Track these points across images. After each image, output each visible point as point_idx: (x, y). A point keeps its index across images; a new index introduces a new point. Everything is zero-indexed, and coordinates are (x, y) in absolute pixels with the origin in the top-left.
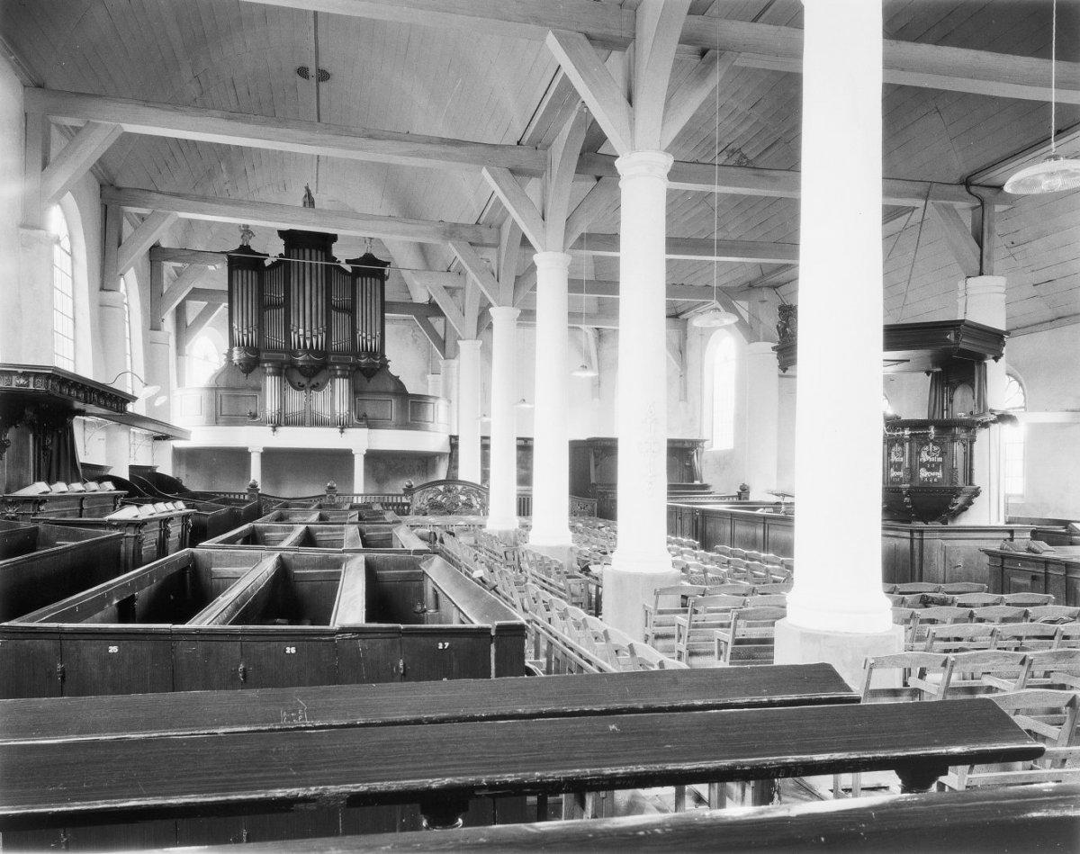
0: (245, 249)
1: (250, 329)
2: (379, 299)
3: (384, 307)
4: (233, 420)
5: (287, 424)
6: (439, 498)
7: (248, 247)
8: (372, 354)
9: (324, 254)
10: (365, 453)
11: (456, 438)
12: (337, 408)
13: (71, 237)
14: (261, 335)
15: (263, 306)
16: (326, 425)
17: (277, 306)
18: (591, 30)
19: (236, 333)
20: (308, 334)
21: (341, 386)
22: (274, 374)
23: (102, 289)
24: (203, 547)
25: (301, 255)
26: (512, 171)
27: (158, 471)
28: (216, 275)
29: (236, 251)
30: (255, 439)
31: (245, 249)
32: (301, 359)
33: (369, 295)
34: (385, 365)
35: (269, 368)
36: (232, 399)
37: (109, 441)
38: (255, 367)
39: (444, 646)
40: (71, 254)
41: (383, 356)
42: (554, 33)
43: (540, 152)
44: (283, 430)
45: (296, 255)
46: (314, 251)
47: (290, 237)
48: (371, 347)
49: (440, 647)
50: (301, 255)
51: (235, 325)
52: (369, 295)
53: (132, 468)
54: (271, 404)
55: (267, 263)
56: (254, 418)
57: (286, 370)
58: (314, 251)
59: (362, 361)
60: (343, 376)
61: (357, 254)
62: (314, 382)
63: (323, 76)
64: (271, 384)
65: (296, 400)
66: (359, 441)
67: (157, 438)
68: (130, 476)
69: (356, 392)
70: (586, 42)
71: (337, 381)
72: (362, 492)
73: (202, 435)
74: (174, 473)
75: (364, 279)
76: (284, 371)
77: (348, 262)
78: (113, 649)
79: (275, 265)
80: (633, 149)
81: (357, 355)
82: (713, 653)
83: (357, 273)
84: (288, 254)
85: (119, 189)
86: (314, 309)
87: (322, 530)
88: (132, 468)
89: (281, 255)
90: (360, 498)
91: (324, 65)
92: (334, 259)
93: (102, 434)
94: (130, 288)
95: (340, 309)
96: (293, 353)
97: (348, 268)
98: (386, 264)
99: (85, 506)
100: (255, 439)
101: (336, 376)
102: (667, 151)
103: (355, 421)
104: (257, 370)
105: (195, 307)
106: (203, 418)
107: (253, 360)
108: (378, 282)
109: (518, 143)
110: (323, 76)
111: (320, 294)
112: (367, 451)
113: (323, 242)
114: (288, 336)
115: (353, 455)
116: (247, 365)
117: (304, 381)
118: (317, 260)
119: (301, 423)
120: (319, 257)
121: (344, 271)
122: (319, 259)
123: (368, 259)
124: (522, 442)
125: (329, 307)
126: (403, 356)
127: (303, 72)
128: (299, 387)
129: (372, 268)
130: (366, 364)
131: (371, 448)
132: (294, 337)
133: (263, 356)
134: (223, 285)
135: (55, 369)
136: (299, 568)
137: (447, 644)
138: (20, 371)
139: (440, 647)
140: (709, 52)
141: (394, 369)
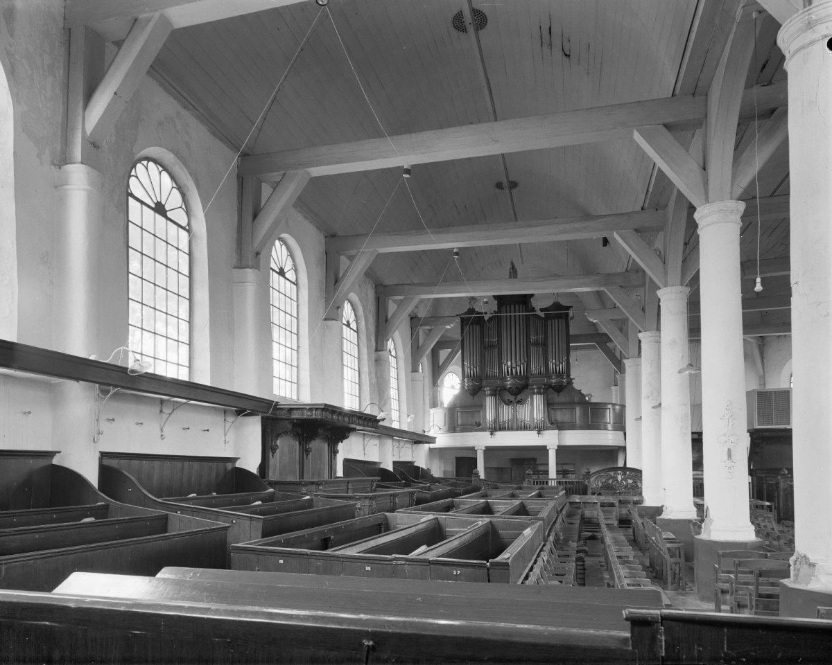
0: (471, 311)
1: (522, 360)
2: (564, 334)
3: (569, 338)
4: (466, 428)
5: (501, 429)
6: (610, 481)
7: (473, 309)
8: (560, 375)
9: (524, 306)
10: (484, 449)
11: (700, 434)
12: (535, 417)
13: (357, 320)
14: (482, 369)
15: (485, 347)
16: (527, 430)
17: (493, 346)
18: (667, 121)
19: (466, 369)
20: (514, 365)
21: (538, 400)
22: (491, 395)
23: (377, 350)
24: (399, 512)
25: (513, 309)
26: (637, 230)
27: (415, 464)
28: (452, 328)
29: (466, 313)
30: (480, 441)
31: (471, 311)
32: (509, 383)
33: (557, 332)
34: (570, 382)
35: (487, 391)
36: (464, 415)
37: (381, 446)
38: (479, 391)
39: (457, 573)
40: (357, 332)
41: (568, 376)
42: (637, 130)
43: (660, 211)
44: (499, 434)
45: (505, 311)
46: (517, 306)
47: (502, 300)
48: (516, 372)
49: (455, 573)
50: (513, 309)
51: (465, 363)
52: (557, 332)
53: (395, 463)
54: (489, 415)
55: (486, 318)
56: (478, 427)
57: (499, 391)
58: (517, 306)
59: (553, 381)
60: (539, 393)
61: (548, 303)
62: (519, 398)
63: (513, 185)
64: (489, 402)
65: (507, 413)
66: (551, 440)
67: (415, 443)
68: (394, 468)
69: (549, 405)
70: (664, 129)
71: (535, 396)
72: (555, 477)
73: (443, 440)
74: (426, 464)
75: (553, 321)
76: (498, 392)
77: (542, 310)
78: (281, 561)
79: (490, 319)
80: (707, 200)
81: (550, 377)
82: (747, 606)
83: (548, 317)
84: (500, 311)
85: (386, 286)
86: (526, 344)
87: (499, 504)
88: (395, 463)
89: (495, 312)
90: (553, 481)
91: (512, 179)
92: (533, 310)
93: (376, 442)
94: (397, 345)
95: (536, 344)
96: (504, 379)
97: (542, 314)
98: (568, 308)
99: (350, 487)
100: (480, 441)
101: (534, 393)
102: (740, 199)
103: (549, 425)
104: (480, 393)
105: (443, 354)
106: (445, 428)
107: (475, 389)
108: (564, 321)
109: (642, 209)
110: (513, 185)
111: (522, 337)
112: (558, 446)
113: (524, 300)
114: (500, 368)
115: (548, 450)
116: (474, 390)
117: (512, 398)
118: (510, 312)
119: (511, 429)
120: (517, 309)
121: (539, 317)
122: (521, 310)
123: (557, 306)
124: (696, 436)
125: (528, 343)
126: (586, 375)
127: (499, 186)
128: (509, 403)
129: (559, 312)
130: (555, 383)
131: (563, 444)
132: (505, 368)
133: (484, 383)
134: (458, 336)
135: (326, 405)
136: (504, 529)
137: (459, 572)
138: (308, 407)
139: (455, 573)
140: (778, 110)
141: (577, 385)
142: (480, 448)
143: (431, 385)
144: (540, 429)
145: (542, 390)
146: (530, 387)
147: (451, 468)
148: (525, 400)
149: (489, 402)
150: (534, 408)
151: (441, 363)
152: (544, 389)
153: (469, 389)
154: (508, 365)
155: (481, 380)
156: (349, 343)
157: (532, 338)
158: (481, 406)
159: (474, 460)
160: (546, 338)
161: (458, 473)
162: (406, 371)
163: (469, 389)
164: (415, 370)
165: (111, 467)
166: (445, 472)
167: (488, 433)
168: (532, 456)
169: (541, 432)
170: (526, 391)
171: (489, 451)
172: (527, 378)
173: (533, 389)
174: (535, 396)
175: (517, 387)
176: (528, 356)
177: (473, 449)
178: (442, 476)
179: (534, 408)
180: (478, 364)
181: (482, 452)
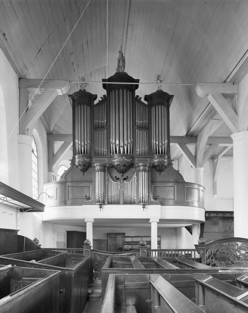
1: (126, 142)
4: (75, 202)
8: (162, 154)
9: (104, 173)
15: (95, 128)
27: (19, 233)
30: (89, 213)
51: (76, 141)
56: (87, 200)
57: (108, 168)
64: (98, 177)
65: (115, 188)
69: (152, 182)
90: (154, 252)
95: (142, 128)
100: (89, 213)
103: (152, 200)
104: (90, 169)
106: (58, 201)
116: (84, 165)
117: (119, 175)
119: (118, 203)
125: (134, 126)
132: (113, 147)
142: (89, 220)
143: (48, 171)
144: (144, 204)
145: (147, 168)
146: (136, 165)
147: (63, 239)
148: (131, 177)
149: (98, 177)
150: (139, 183)
151: (55, 152)
152: (149, 167)
153: (80, 165)
154: (115, 142)
155: (90, 157)
156: (35, 187)
157: (138, 122)
158: (92, 181)
159: (83, 235)
160: (150, 123)
161: (69, 244)
162: (9, 130)
163: (80, 165)
164: (23, 131)
165: (75, 237)
166: (58, 243)
167: (97, 207)
168: (122, 232)
169: (146, 206)
170: (132, 170)
171: (98, 224)
172: (132, 157)
173: (139, 166)
174: (140, 174)
175: (125, 165)
176: (134, 137)
177: (83, 224)
178: (55, 247)
179: (139, 183)
180: (88, 141)
181: (91, 224)
